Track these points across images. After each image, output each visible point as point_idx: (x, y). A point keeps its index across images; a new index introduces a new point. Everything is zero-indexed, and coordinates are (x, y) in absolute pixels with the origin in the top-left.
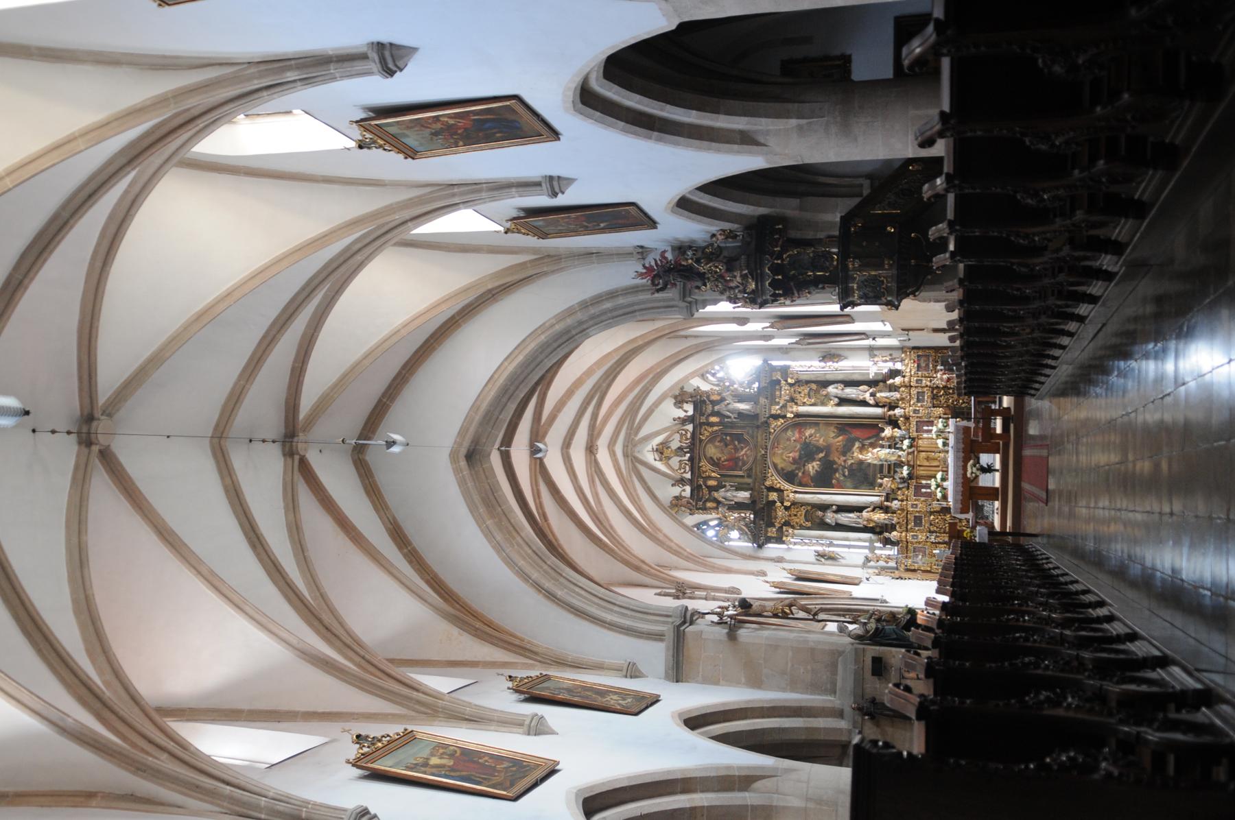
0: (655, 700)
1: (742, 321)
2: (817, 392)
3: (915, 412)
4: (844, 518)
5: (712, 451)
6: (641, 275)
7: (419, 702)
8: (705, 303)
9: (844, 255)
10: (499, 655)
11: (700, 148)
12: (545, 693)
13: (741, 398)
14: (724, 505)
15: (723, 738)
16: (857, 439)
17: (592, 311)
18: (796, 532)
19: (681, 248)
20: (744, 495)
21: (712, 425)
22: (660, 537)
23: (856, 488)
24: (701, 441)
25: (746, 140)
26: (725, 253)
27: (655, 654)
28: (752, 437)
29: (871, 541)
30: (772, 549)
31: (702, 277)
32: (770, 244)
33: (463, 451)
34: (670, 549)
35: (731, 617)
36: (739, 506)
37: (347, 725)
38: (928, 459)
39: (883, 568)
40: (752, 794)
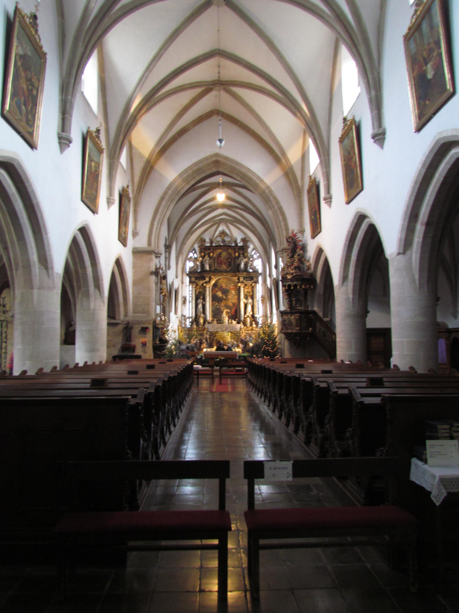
0: (125, 245)
1: (276, 267)
4: (200, 306)
5: (224, 254)
6: (293, 232)
9: (301, 313)
10: (137, 179)
11: (342, 260)
12: (123, 202)
16: (231, 310)
18: (194, 288)
19: (304, 248)
21: (235, 253)
22: (188, 236)
24: (228, 249)
25: (344, 278)
26: (302, 265)
29: (191, 317)
30: (187, 279)
31: (292, 257)
32: (304, 287)
37: (103, 124)
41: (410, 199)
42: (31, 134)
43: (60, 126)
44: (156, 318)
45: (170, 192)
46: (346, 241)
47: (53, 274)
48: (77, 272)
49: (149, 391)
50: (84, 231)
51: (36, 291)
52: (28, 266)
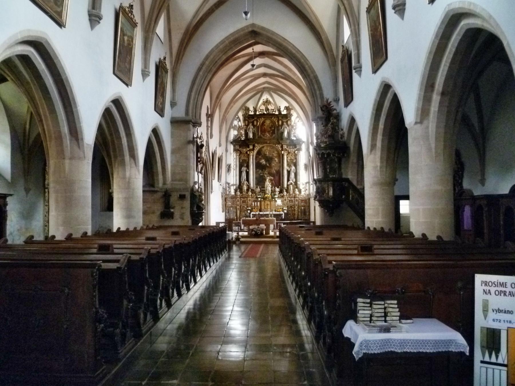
0: (162, 115)
2: (292, 162)
3: (285, 200)
5: (268, 122)
7: (150, 24)
8: (317, 126)
13: (289, 134)
14: (246, 128)
15: (150, 144)
17: (314, 81)
19: (338, 117)
20: (251, 135)
21: (278, 122)
22: (232, 104)
23: (256, 178)
24: (272, 118)
27: (180, 113)
28: (274, 138)
29: (236, 185)
30: (231, 148)
31: (326, 126)
33: (255, 29)
34: (227, 108)
35: (197, 141)
36: (246, 134)
38: (268, 205)
39: (226, 189)
40: (128, 159)
41: (425, 69)
42: (60, 14)
43: (91, 4)
44: (194, 186)
45: (207, 63)
46: (373, 110)
47: (83, 145)
48: (113, 142)
49: (141, 256)
50: (117, 102)
51: (67, 161)
52: (59, 138)
